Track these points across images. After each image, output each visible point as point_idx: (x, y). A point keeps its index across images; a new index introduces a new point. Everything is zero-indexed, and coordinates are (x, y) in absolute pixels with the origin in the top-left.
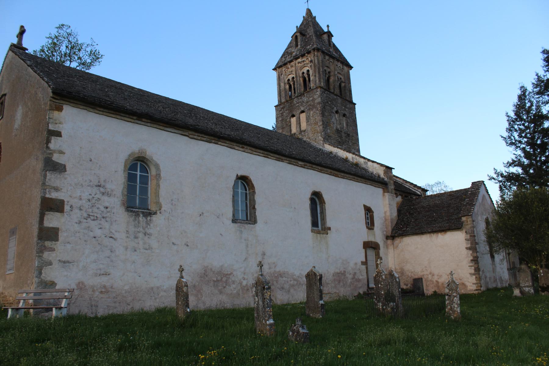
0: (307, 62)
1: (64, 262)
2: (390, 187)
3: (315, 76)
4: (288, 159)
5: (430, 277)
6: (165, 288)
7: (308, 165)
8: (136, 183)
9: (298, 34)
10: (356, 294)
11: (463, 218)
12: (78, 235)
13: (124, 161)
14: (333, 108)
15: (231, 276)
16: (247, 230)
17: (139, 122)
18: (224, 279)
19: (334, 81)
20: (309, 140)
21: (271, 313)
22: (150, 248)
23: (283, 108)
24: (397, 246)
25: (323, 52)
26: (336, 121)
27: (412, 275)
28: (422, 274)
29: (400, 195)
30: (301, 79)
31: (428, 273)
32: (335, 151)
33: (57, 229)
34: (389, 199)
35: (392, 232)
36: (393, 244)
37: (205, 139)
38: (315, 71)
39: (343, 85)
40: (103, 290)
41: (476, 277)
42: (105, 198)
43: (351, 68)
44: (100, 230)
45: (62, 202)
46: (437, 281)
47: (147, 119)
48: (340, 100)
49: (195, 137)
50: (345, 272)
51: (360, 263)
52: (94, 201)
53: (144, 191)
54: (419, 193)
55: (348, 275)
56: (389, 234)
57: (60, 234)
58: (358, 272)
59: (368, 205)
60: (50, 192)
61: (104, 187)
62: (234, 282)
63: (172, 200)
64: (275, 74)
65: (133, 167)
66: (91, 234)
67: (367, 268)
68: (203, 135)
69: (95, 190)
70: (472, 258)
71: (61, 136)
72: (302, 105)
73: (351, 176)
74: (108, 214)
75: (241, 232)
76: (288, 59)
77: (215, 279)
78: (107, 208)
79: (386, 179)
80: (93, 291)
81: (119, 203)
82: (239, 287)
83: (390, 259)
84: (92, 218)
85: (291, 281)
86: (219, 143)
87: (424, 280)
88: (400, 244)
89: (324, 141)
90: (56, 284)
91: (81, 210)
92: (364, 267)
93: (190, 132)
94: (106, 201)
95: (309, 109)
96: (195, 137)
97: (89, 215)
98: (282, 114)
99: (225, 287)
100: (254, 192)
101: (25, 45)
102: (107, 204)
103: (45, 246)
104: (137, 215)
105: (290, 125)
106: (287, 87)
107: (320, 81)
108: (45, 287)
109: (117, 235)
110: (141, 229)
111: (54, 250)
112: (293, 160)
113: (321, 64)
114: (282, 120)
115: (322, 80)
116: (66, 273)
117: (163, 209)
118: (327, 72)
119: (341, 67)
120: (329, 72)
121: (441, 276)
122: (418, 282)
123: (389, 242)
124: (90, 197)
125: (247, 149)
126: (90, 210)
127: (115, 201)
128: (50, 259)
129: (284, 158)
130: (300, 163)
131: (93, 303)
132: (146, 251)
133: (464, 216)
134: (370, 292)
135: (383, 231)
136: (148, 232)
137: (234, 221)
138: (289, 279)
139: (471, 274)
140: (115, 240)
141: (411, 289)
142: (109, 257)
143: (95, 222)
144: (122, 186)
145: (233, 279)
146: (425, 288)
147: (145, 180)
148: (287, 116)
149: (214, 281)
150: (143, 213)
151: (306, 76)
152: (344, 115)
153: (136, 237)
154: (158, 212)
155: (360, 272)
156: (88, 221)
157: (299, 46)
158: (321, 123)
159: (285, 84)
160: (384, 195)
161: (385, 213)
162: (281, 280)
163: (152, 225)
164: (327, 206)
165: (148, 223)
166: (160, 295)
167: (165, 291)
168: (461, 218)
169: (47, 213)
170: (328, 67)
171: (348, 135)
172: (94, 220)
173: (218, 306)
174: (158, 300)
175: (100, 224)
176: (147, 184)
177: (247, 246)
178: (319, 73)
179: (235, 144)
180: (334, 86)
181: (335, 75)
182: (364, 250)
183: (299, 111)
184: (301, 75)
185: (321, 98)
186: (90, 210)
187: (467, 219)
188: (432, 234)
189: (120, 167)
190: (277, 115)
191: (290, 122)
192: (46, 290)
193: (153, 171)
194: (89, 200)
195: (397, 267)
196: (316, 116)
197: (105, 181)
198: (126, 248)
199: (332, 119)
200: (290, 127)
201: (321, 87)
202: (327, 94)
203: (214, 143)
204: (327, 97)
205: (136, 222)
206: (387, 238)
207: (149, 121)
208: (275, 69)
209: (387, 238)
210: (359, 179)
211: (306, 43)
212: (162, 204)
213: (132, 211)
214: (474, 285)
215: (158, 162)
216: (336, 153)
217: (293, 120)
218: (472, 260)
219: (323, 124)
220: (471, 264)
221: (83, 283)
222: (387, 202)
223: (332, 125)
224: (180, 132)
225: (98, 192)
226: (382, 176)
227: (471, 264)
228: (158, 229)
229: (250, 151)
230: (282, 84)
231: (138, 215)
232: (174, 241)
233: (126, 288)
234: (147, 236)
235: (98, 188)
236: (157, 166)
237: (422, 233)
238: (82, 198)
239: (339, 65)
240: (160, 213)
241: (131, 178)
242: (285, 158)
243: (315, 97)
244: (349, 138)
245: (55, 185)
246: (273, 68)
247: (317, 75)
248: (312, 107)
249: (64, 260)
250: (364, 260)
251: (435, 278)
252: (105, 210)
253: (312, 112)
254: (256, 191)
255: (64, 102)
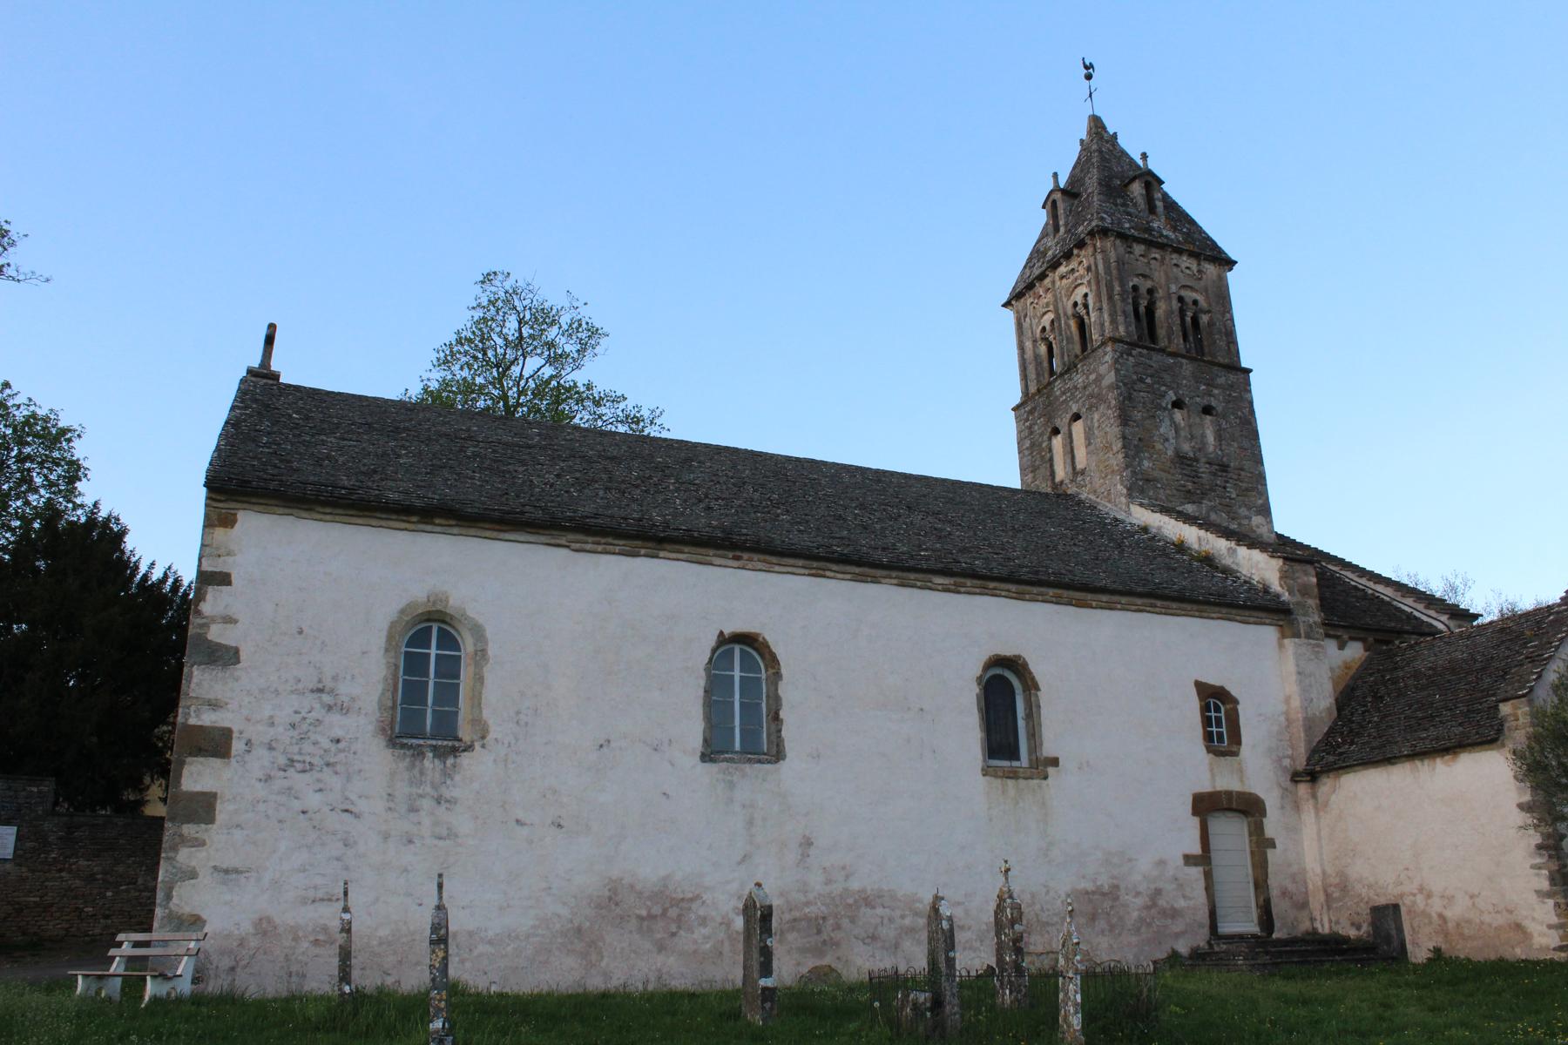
0: (1082, 271)
1: (227, 871)
2: (1301, 619)
3: (1100, 309)
4: (894, 574)
5: (1420, 899)
6: (490, 934)
7: (969, 582)
8: (427, 675)
9: (1058, 196)
10: (1161, 955)
11: (1502, 706)
12: (261, 807)
13: (385, 626)
14: (1163, 396)
15: (694, 906)
16: (753, 781)
17: (429, 528)
18: (673, 912)
19: (1169, 313)
20: (1092, 497)
21: (443, 1004)
22: (452, 835)
23: (1031, 412)
24: (1326, 804)
25: (1122, 236)
26: (1174, 432)
27: (1372, 894)
28: (1398, 890)
29: (1352, 639)
30: (1072, 323)
31: (1413, 887)
32: (1157, 524)
33: (214, 796)
34: (1298, 657)
35: (1309, 759)
36: (1314, 796)
37: (617, 549)
38: (1098, 296)
39: (1204, 319)
40: (321, 937)
41: (1557, 905)
42: (335, 718)
43: (1230, 263)
44: (318, 796)
45: (227, 734)
46: (1441, 916)
47: (447, 518)
48: (1187, 368)
49: (588, 547)
50: (1117, 887)
51: (1181, 861)
52: (305, 727)
53: (448, 693)
54: (1441, 626)
55: (1126, 898)
56: (1301, 764)
57: (218, 807)
58: (1169, 887)
59: (1213, 680)
60: (197, 711)
61: (332, 691)
62: (703, 921)
63: (518, 713)
64: (1009, 316)
65: (420, 639)
66: (297, 805)
67: (1208, 875)
68: (610, 540)
69: (310, 700)
70: (1538, 839)
71: (229, 583)
72: (1073, 397)
73: (1139, 601)
74: (342, 755)
75: (731, 785)
76: (1037, 272)
77: (644, 913)
78: (338, 741)
79: (1286, 597)
80: (296, 939)
81: (371, 728)
82: (722, 935)
83: (1306, 844)
84: (299, 766)
85: (903, 917)
86: (662, 554)
87: (1403, 910)
88: (1333, 797)
89: (1130, 496)
90: (204, 922)
91: (271, 748)
92: (1196, 873)
93: (571, 536)
94: (338, 724)
95: (1090, 409)
96: (588, 547)
97: (292, 761)
98: (1030, 428)
99: (673, 934)
100: (778, 676)
101: (274, 367)
102: (339, 733)
103: (181, 835)
104: (419, 753)
105: (1051, 459)
106: (1043, 349)
107: (1113, 321)
108: (178, 929)
109: (362, 806)
110: (428, 789)
111: (203, 844)
112: (912, 576)
113: (1115, 272)
114: (1033, 445)
115: (1120, 319)
116: (228, 897)
117: (491, 736)
118: (1143, 290)
119: (1194, 267)
120: (1150, 291)
121: (1451, 899)
122: (1387, 915)
123: (1303, 789)
124: (297, 718)
125: (750, 560)
126: (296, 749)
127: (361, 728)
128: (193, 863)
129: (879, 573)
130: (939, 580)
131: (294, 969)
132: (441, 843)
133: (1505, 700)
134: (1216, 949)
135: (1280, 760)
136: (447, 794)
137: (708, 756)
138: (898, 912)
139: (1541, 894)
140: (357, 816)
141: (1371, 939)
142: (338, 859)
143: (306, 776)
144: (380, 687)
145: (701, 912)
146: (1408, 938)
147: (450, 668)
148: (1041, 435)
149: (641, 918)
150: (434, 748)
151: (1080, 309)
152: (1207, 410)
153: (413, 810)
154: (477, 745)
155: (1180, 886)
156: (288, 774)
157: (1062, 230)
158: (1120, 445)
159: (1035, 341)
160: (1281, 646)
161: (1287, 700)
162: (868, 916)
163: (457, 778)
164: (1044, 696)
165: (447, 774)
166: (476, 953)
167: (490, 942)
168: (1496, 708)
169: (189, 759)
170: (1144, 276)
171: (1224, 468)
172: (304, 771)
173: (650, 988)
174: (468, 965)
175: (319, 780)
176: (458, 677)
177: (750, 823)
178: (1110, 298)
179: (711, 552)
180: (1170, 328)
181: (1169, 296)
182: (1196, 820)
183: (1069, 416)
184: (1070, 311)
185: (1117, 371)
186: (296, 749)
187: (1516, 708)
188: (1418, 763)
189: (377, 640)
190: (1019, 432)
191: (1050, 450)
192: (178, 935)
193: (468, 645)
194: (293, 726)
195: (1329, 870)
196: (1106, 423)
197: (335, 678)
198: (386, 837)
199: (1158, 428)
200: (1052, 466)
201: (1114, 340)
202: (1141, 355)
203: (646, 556)
204: (1137, 364)
205: (416, 772)
206: (1296, 777)
207: (452, 522)
208: (1007, 304)
209: (1296, 777)
210: (1174, 605)
211: (1078, 218)
212: (490, 722)
213: (403, 746)
214: (1553, 932)
215: (481, 620)
216: (1159, 528)
217: (1057, 442)
218: (1539, 847)
219: (1124, 447)
220: (1538, 860)
221: (269, 920)
222: (1290, 666)
223: (1159, 446)
224: (543, 539)
225: (318, 706)
226: (1276, 586)
227: (1538, 860)
228: (476, 786)
229: (760, 565)
230: (1028, 345)
231: (422, 755)
232: (520, 815)
233: (383, 932)
234: (444, 805)
235: (316, 695)
236: (478, 632)
237: (1389, 760)
238: (277, 721)
239: (1183, 266)
240: (483, 746)
241: (415, 664)
242: (885, 573)
243: (1103, 369)
244: (1227, 476)
245: (211, 696)
246: (1005, 300)
247: (1105, 306)
248: (1096, 400)
249: (225, 866)
250: (1196, 849)
251: (1436, 906)
252: (333, 748)
253: (1096, 416)
254: (784, 671)
255: (238, 505)
